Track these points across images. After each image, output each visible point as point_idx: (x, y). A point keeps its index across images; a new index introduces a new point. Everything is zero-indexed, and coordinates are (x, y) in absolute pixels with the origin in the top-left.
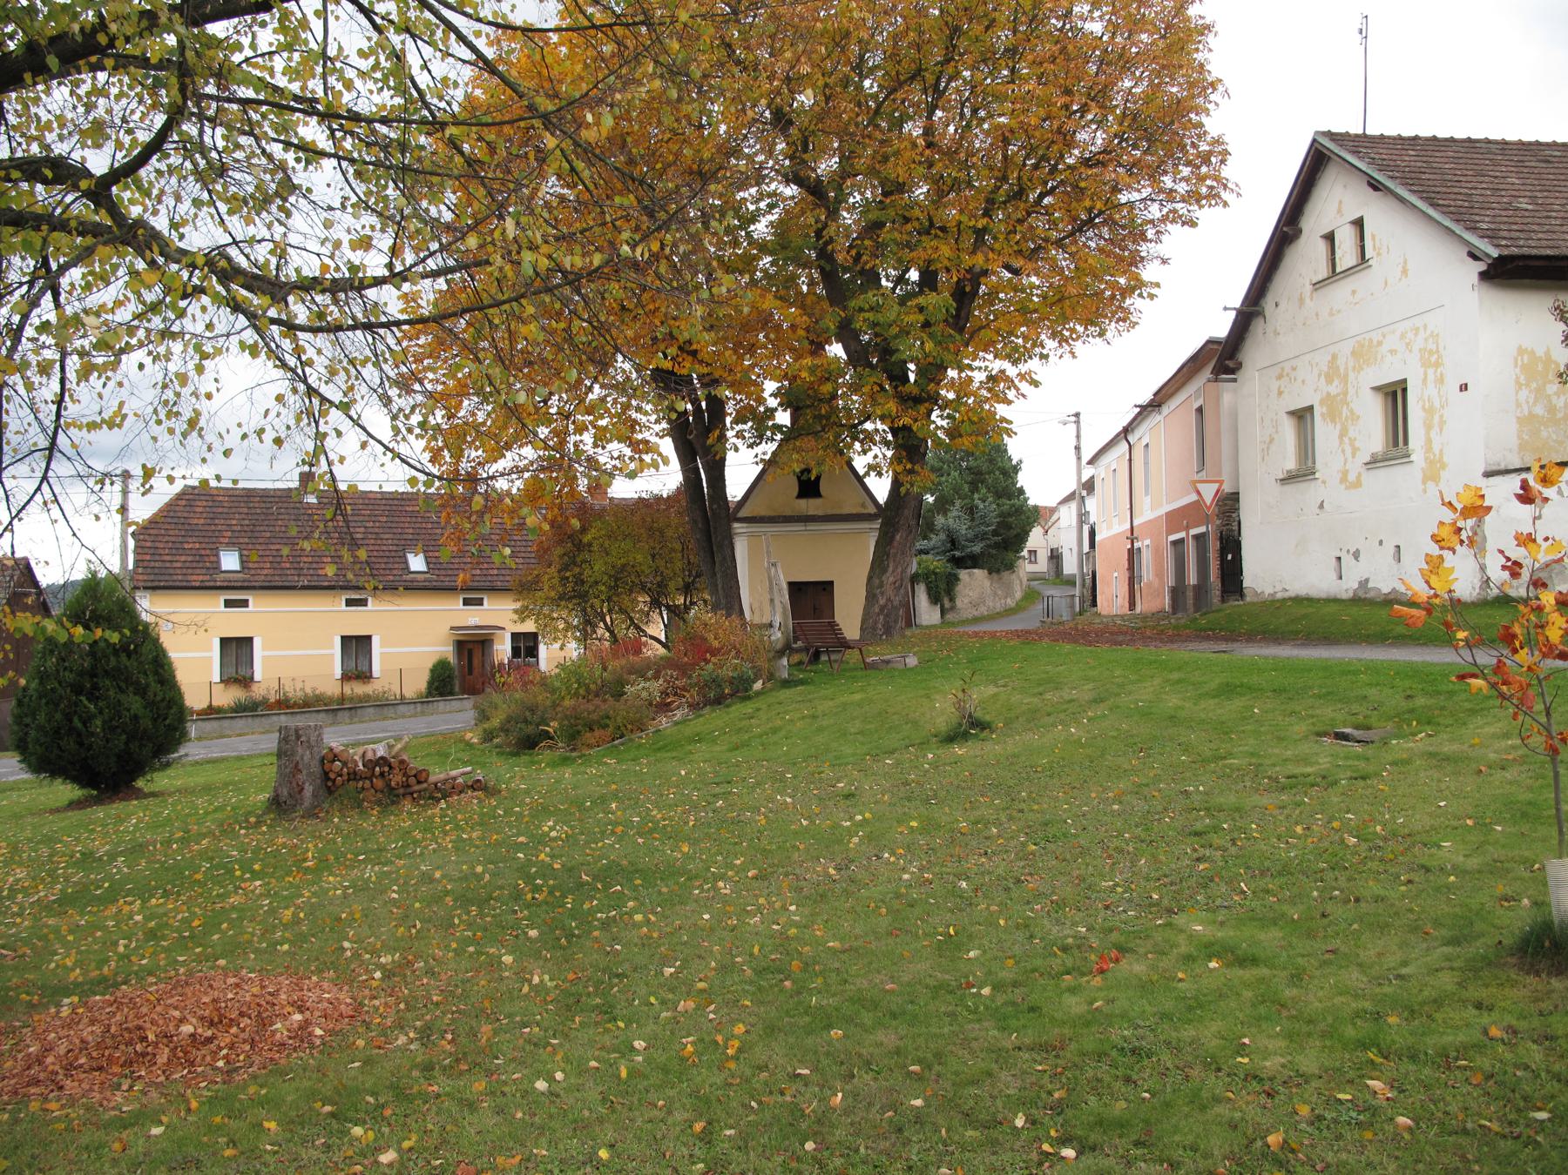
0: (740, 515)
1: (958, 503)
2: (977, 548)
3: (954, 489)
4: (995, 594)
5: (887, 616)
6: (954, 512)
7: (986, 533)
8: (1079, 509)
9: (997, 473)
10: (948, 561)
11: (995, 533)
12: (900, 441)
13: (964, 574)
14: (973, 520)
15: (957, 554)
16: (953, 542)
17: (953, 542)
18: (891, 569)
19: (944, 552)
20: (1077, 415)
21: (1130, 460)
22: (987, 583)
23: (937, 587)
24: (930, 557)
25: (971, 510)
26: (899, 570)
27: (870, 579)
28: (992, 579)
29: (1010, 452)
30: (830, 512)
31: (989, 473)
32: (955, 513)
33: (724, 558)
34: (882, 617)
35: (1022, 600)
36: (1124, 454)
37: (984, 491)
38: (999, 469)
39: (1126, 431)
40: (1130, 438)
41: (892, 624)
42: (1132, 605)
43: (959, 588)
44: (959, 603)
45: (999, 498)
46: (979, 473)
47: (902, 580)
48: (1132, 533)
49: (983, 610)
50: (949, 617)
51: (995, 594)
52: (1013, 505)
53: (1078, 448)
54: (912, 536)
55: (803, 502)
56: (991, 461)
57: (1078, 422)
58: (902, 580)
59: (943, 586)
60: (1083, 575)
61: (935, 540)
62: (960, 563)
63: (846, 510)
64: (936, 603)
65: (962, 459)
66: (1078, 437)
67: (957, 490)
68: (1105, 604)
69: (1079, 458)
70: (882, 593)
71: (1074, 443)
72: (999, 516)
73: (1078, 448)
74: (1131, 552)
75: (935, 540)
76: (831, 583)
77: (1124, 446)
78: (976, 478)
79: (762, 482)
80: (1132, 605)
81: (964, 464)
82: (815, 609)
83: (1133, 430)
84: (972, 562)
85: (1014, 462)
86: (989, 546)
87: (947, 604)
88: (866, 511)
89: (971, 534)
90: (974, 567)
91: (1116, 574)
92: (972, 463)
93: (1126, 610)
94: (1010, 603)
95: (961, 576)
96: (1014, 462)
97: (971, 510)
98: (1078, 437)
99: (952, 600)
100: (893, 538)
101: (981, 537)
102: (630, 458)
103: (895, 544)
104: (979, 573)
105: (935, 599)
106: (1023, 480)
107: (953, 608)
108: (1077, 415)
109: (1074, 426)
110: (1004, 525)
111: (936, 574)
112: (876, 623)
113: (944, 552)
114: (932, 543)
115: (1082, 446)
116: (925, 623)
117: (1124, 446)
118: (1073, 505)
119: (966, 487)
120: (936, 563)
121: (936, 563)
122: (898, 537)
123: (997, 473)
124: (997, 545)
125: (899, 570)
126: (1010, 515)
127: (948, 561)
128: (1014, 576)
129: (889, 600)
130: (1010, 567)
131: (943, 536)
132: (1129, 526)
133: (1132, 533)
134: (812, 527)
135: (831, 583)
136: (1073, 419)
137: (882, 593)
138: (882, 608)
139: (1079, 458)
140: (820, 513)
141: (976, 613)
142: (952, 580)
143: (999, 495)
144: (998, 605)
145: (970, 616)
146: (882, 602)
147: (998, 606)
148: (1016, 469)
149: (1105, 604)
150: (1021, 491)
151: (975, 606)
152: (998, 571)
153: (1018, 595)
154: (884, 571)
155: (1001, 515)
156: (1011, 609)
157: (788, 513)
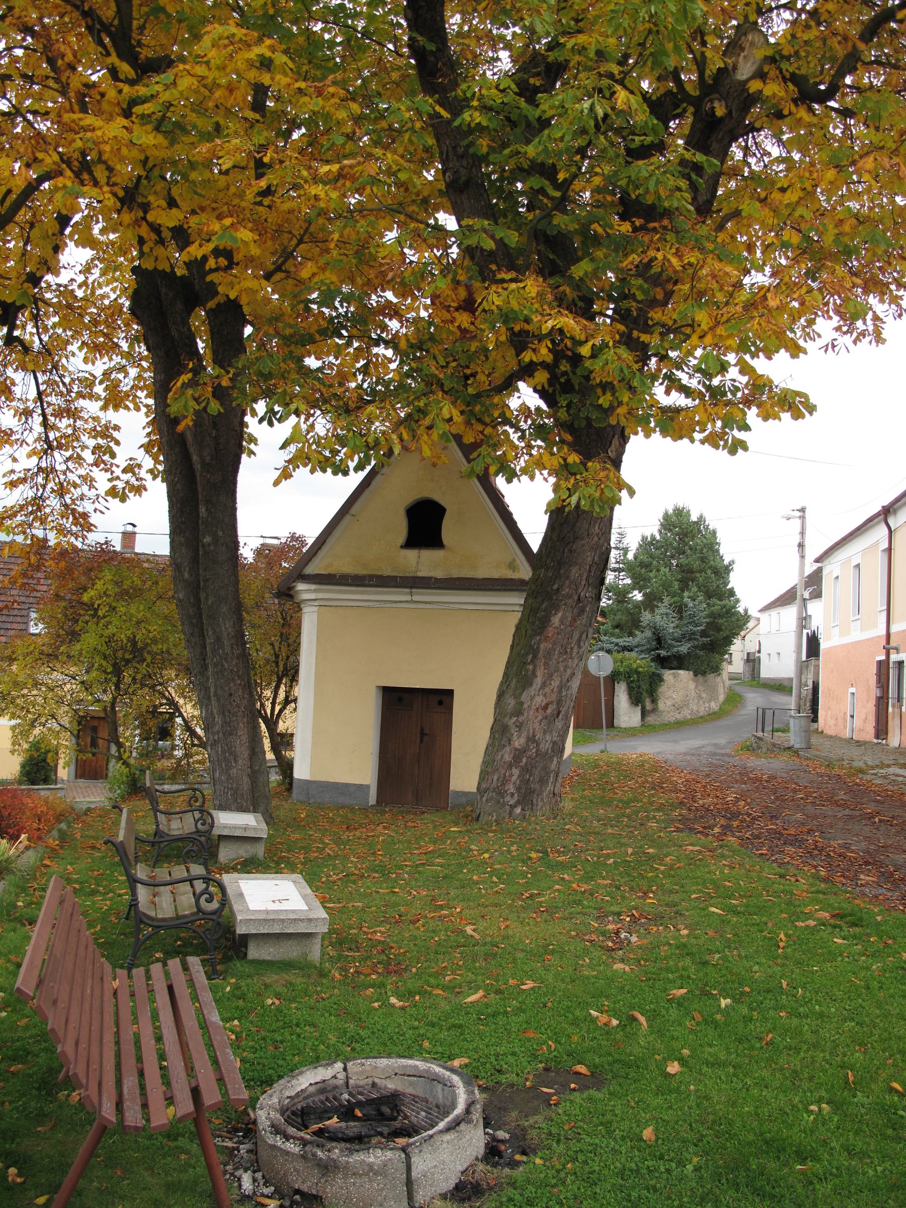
0: (310, 570)
1: (667, 600)
2: (684, 648)
3: (663, 586)
4: (700, 697)
5: (526, 770)
6: (663, 608)
7: (694, 634)
8: (800, 612)
9: (709, 572)
10: (653, 660)
11: (703, 634)
12: (563, 414)
13: (668, 675)
14: (681, 618)
15: (663, 653)
16: (659, 640)
17: (659, 640)
18: (538, 681)
19: (649, 651)
20: (803, 510)
21: (889, 550)
22: (692, 685)
23: (639, 687)
24: (633, 654)
25: (680, 609)
26: (555, 683)
27: (501, 695)
28: (697, 682)
29: (722, 551)
30: (456, 574)
31: (700, 571)
32: (663, 610)
33: (218, 639)
34: (516, 772)
35: (724, 703)
36: (877, 543)
37: (695, 589)
38: (710, 568)
39: (887, 512)
40: (891, 521)
41: (535, 786)
42: (881, 730)
43: (663, 689)
44: (661, 705)
45: (710, 598)
46: (691, 571)
47: (559, 702)
48: (888, 642)
49: (686, 714)
50: (650, 719)
51: (700, 697)
52: (725, 606)
53: (801, 546)
54: (584, 619)
55: (412, 554)
56: (703, 560)
57: (803, 518)
58: (559, 702)
59: (645, 686)
60: (801, 685)
61: (641, 637)
62: (665, 662)
63: (483, 572)
64: (637, 705)
65: (672, 557)
66: (802, 533)
67: (666, 586)
68: (831, 722)
69: (803, 557)
70: (520, 726)
71: (797, 539)
72: (709, 616)
73: (801, 546)
74: (883, 667)
75: (641, 637)
76: (450, 693)
77: (881, 532)
78: (687, 576)
79: (348, 518)
80: (881, 730)
81: (674, 562)
82: (423, 734)
83: (895, 512)
84: (677, 662)
85: (726, 562)
86: (695, 647)
87: (649, 706)
88: (515, 576)
89: (678, 633)
90: (680, 668)
91: (853, 690)
92: (683, 560)
93: (868, 733)
94: (714, 706)
95: (665, 677)
96: (726, 562)
97: (680, 609)
98: (802, 533)
99: (654, 701)
100: (545, 622)
101: (688, 637)
102: (151, 471)
103: (550, 632)
104: (684, 675)
105: (636, 699)
106: (735, 581)
107: (654, 710)
108: (803, 510)
109: (798, 522)
110: (713, 626)
111: (638, 673)
112: (505, 781)
113: (649, 651)
114: (637, 640)
115: (807, 543)
116: (623, 725)
117: (881, 532)
118: (790, 613)
119: (676, 585)
120: (640, 661)
121: (640, 661)
122: (556, 620)
123: (709, 572)
124: (703, 647)
125: (555, 683)
126: (720, 616)
127: (653, 660)
128: (718, 679)
129: (532, 739)
130: (716, 670)
131: (648, 634)
132: (884, 632)
133: (888, 642)
134: (421, 596)
135: (450, 693)
136: (798, 514)
137: (520, 726)
138: (518, 754)
139: (803, 557)
140: (439, 574)
141: (679, 717)
142: (655, 681)
143: (709, 595)
144: (702, 709)
145: (672, 719)
146: (519, 742)
147: (702, 709)
148: (728, 569)
149: (831, 722)
150: (732, 593)
151: (679, 709)
152: (704, 673)
153: (722, 698)
154: (526, 682)
155: (711, 615)
156: (715, 713)
157: (387, 571)
